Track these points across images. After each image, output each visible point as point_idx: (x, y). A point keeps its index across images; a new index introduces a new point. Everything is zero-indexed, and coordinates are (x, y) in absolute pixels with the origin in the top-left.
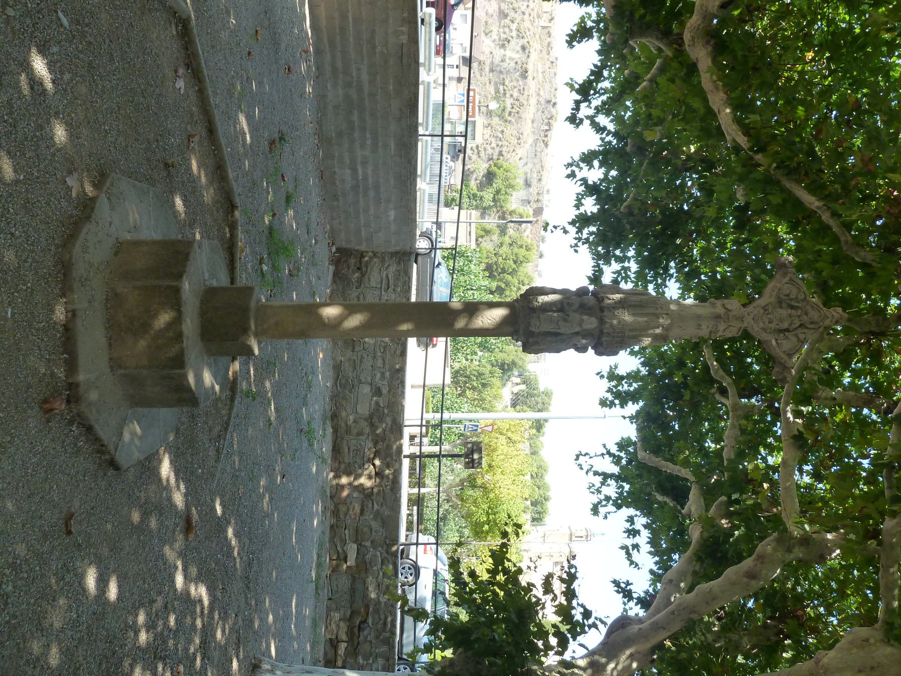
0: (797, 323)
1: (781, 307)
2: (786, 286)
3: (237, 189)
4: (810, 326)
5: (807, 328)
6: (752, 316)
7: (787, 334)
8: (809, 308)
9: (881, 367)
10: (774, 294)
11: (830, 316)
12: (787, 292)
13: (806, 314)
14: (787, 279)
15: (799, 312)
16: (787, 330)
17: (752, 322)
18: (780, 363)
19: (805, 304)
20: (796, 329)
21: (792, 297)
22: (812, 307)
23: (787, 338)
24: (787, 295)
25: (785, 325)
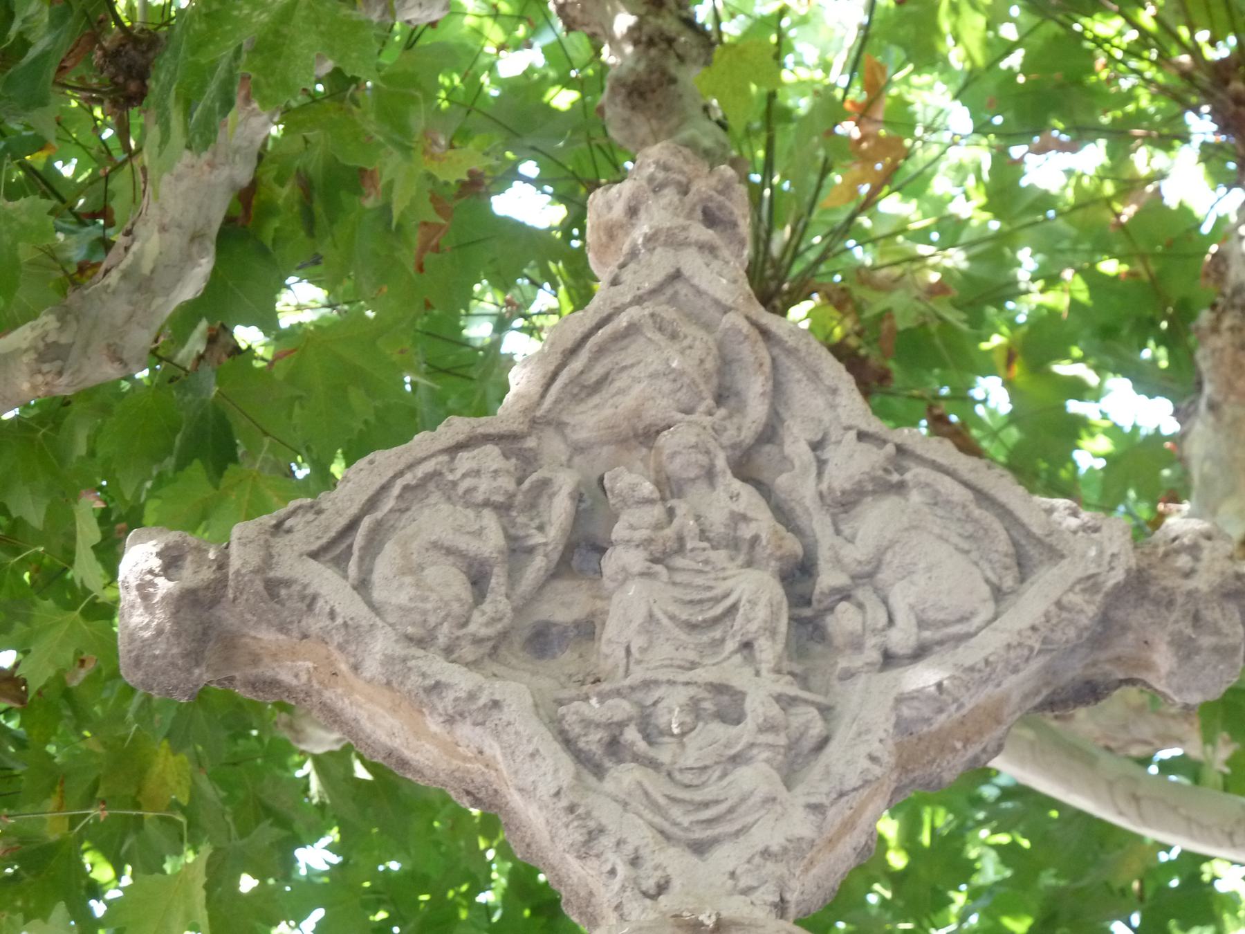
0: (729, 498)
1: (587, 630)
2: (390, 586)
3: (391, 474)
4: (757, 411)
5: (770, 433)
6: (675, 861)
7: (828, 578)
8: (588, 420)
9: (986, 290)
10: (461, 680)
11: (660, 263)
12: (449, 582)
13: (648, 436)
14: (330, 585)
15: (632, 480)
16: (798, 574)
17: (726, 857)
18: (1106, 629)
19: (553, 446)
20: (783, 514)
21: (491, 541)
22: (587, 389)
23: (867, 575)
24: (478, 579)
25: (757, 592)
